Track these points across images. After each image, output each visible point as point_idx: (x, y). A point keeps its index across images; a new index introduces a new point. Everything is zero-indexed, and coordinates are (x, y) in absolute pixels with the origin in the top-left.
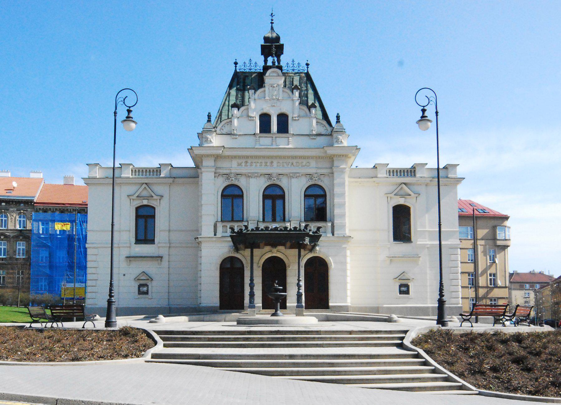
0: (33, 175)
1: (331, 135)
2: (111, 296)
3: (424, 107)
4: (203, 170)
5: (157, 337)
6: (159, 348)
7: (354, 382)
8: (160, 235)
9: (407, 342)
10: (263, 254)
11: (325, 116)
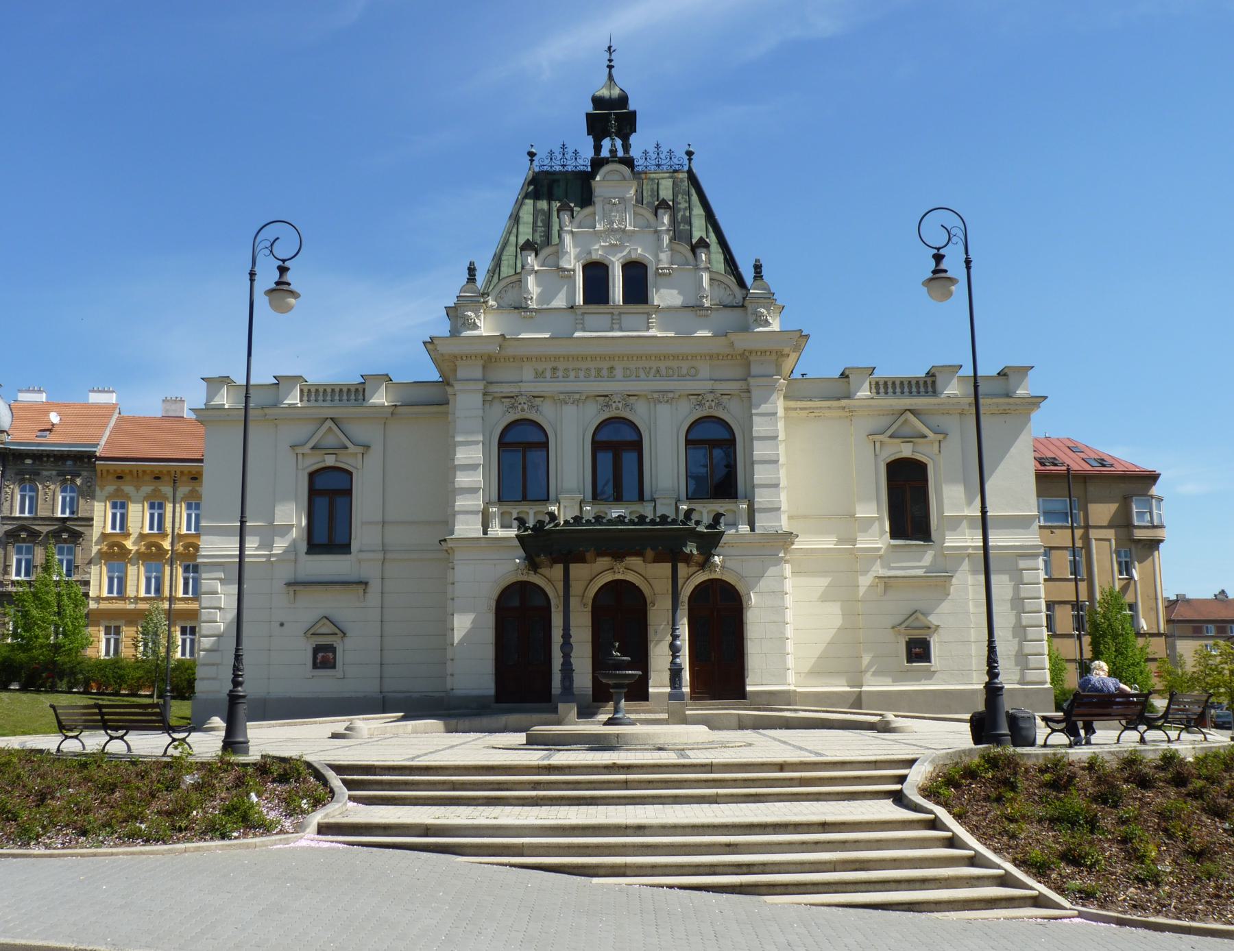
0: (94, 398)
1: (743, 306)
2: (236, 683)
3: (938, 249)
4: (458, 386)
5: (335, 781)
6: (344, 809)
7: (783, 889)
8: (363, 535)
9: (911, 791)
10: (593, 575)
11: (730, 261)
